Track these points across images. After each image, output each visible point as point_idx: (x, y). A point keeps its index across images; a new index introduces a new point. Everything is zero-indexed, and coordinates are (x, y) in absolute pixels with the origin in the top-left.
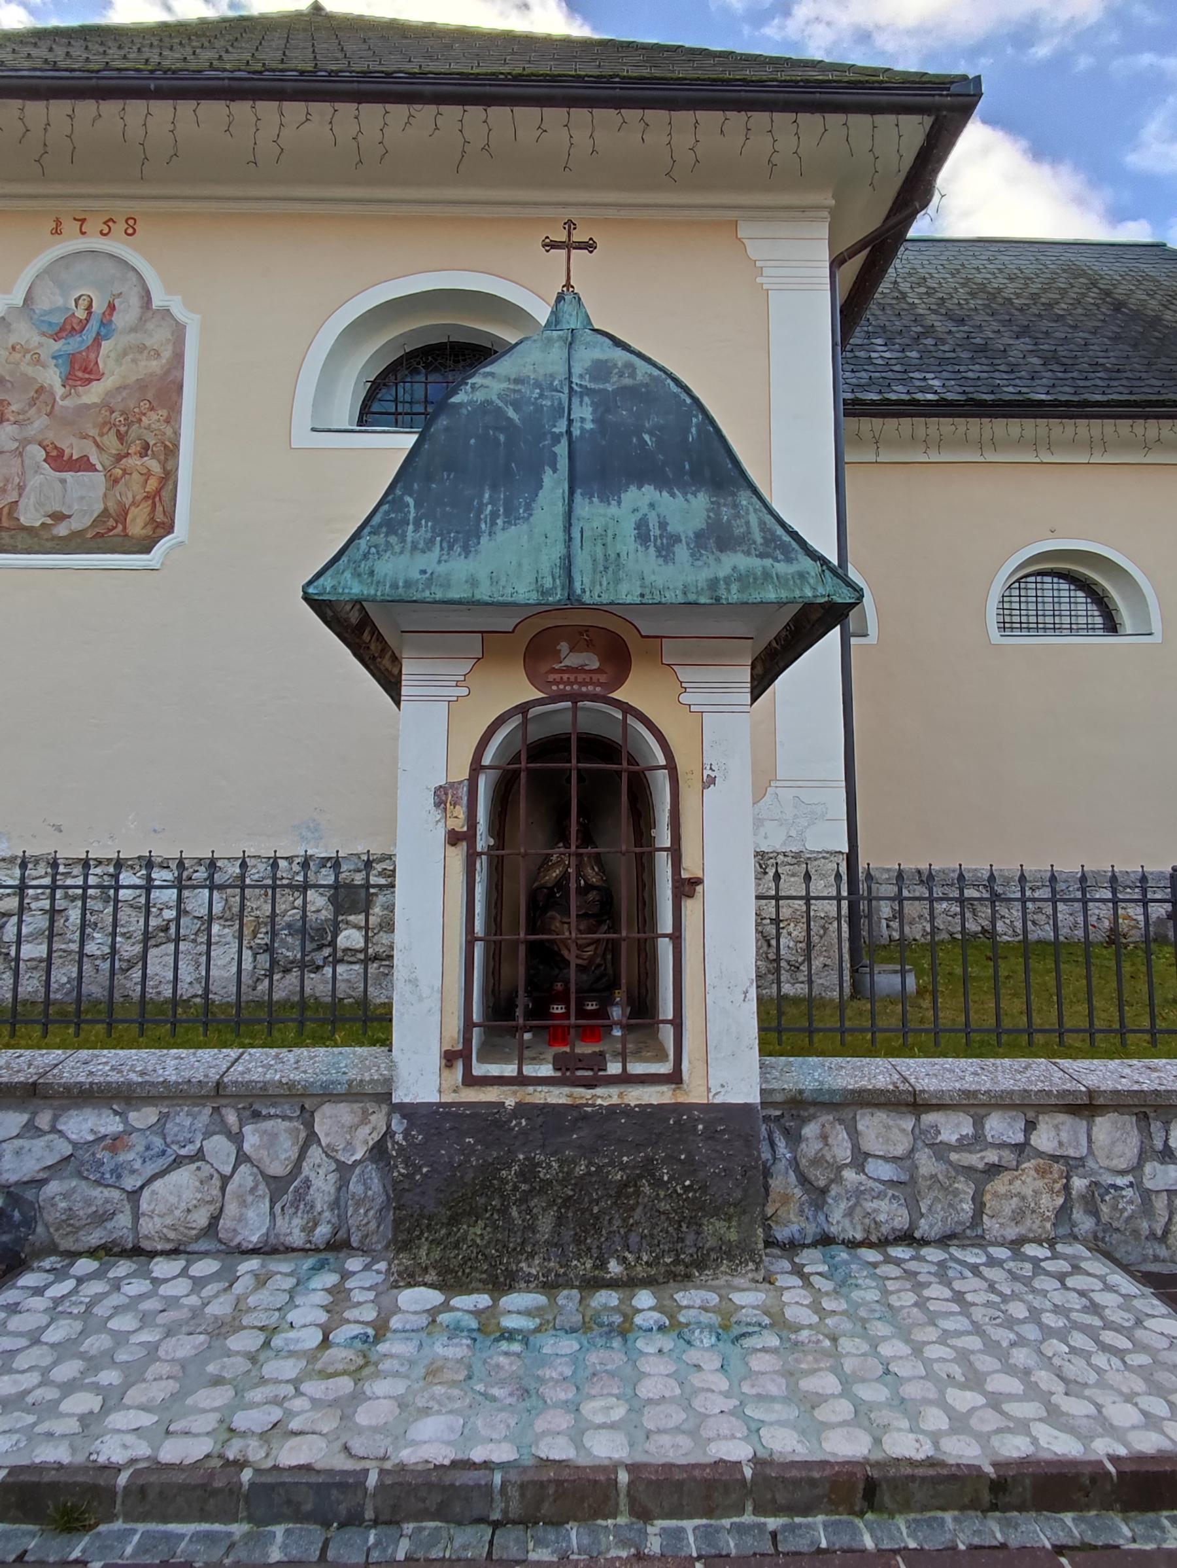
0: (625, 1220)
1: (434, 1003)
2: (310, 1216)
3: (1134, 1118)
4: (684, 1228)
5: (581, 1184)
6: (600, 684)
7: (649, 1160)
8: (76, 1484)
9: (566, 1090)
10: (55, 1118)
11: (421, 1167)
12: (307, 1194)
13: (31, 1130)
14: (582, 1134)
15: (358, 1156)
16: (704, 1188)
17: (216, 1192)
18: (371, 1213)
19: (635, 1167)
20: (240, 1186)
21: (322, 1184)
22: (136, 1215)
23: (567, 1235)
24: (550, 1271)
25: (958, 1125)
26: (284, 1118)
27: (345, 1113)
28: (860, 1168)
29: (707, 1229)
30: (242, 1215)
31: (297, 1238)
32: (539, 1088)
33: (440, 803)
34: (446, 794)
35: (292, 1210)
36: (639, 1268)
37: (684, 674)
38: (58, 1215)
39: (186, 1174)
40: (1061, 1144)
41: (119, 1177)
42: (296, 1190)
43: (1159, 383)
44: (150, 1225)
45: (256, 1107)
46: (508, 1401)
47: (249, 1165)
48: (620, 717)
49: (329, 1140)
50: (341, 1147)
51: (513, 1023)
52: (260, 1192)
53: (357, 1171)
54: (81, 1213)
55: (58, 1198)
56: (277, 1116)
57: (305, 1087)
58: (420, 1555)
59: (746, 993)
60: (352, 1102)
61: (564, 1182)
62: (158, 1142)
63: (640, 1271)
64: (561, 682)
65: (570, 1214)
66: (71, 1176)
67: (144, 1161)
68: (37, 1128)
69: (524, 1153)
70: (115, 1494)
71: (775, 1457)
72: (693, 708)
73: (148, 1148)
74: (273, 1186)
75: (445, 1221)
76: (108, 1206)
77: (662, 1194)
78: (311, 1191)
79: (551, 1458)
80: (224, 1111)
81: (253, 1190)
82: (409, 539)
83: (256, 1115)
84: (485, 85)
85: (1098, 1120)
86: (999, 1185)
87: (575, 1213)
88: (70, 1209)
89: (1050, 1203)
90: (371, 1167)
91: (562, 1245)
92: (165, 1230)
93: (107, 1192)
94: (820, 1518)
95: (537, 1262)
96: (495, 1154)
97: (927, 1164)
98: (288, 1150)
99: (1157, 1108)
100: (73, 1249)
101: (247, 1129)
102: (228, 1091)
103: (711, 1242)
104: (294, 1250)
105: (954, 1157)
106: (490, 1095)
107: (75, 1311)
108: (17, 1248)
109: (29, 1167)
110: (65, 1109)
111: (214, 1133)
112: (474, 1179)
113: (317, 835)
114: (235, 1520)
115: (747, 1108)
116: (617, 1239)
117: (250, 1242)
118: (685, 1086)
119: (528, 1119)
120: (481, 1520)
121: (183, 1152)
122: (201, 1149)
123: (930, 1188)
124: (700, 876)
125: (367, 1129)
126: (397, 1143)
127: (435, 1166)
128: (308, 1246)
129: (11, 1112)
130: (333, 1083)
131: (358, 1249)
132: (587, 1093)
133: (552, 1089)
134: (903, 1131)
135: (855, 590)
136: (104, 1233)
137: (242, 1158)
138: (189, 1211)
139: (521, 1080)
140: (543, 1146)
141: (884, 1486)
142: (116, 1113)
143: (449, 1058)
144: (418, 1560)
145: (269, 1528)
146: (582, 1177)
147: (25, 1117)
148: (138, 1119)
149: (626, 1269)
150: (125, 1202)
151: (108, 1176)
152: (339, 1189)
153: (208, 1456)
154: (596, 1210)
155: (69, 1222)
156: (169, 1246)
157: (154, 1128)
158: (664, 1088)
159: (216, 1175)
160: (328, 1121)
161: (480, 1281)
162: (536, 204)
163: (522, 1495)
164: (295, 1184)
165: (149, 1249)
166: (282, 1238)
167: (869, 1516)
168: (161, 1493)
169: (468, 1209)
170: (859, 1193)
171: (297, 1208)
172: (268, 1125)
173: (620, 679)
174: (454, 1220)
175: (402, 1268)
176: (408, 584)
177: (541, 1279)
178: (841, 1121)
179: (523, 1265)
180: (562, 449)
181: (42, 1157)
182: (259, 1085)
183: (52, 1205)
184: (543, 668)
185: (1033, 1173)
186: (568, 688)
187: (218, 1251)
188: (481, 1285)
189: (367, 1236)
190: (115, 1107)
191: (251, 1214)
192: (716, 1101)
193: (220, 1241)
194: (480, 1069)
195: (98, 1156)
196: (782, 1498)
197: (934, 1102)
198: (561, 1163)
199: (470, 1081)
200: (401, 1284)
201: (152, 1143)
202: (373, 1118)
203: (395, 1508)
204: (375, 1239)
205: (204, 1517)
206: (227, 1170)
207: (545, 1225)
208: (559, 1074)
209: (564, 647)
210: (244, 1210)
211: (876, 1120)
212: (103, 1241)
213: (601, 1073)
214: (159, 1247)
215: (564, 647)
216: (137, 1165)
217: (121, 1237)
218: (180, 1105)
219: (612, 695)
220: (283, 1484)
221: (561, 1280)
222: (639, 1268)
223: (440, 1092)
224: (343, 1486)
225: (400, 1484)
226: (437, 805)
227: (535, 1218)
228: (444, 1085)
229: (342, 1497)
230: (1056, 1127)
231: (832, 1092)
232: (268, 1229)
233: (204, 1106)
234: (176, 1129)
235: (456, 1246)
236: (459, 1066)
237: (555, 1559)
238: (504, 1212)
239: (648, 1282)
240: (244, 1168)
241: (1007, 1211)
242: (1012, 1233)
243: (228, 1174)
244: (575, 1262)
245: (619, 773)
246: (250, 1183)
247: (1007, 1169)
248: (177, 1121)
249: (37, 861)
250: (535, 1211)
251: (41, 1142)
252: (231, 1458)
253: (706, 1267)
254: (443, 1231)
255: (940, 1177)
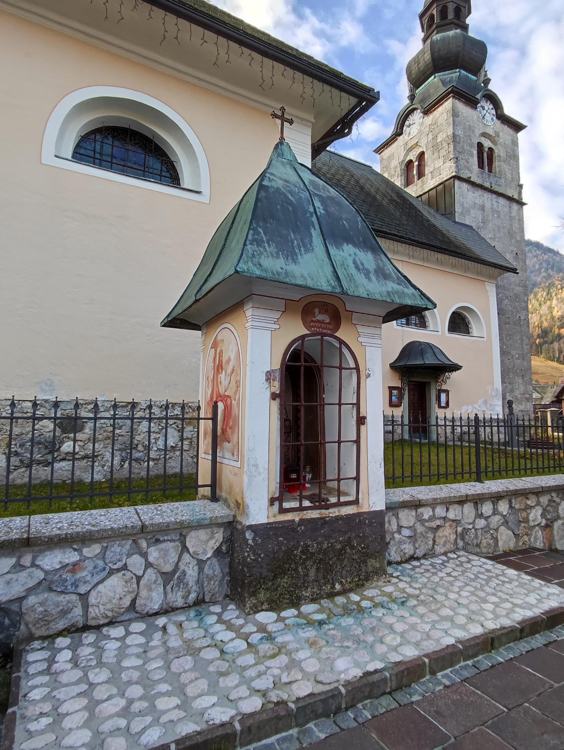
0: (341, 565)
1: (265, 475)
2: (187, 589)
3: (473, 504)
4: (362, 565)
5: (325, 552)
6: (330, 329)
7: (349, 538)
8: (217, 737)
9: (318, 511)
10: (34, 559)
11: (260, 555)
12: (184, 578)
13: (18, 567)
14: (325, 530)
15: (209, 555)
16: (368, 546)
17: (135, 586)
18: (217, 583)
19: (344, 542)
20: (148, 580)
21: (192, 572)
22: (86, 607)
23: (320, 575)
24: (314, 593)
25: (428, 512)
26: (171, 541)
27: (202, 534)
28: (399, 532)
29: (369, 564)
30: (149, 595)
31: (180, 602)
32: (309, 511)
33: (268, 379)
34: (270, 375)
35: (177, 589)
36: (347, 585)
37: (361, 329)
38: (37, 616)
39: (116, 579)
40: (456, 515)
41: (77, 587)
42: (179, 578)
43: (381, 224)
44: (97, 611)
45: (158, 537)
46: (354, 646)
47: (152, 569)
48: (338, 346)
49: (194, 549)
50: (201, 552)
51: (299, 483)
52: (159, 582)
53: (208, 563)
54: (54, 612)
55: (37, 605)
56: (168, 540)
57: (189, 523)
58: (376, 714)
59: (381, 464)
60: (206, 528)
61: (319, 553)
62: (101, 563)
63: (347, 586)
64: (315, 327)
65: (321, 566)
66: (43, 591)
67: (93, 575)
68: (21, 565)
69: (303, 542)
70: (236, 734)
71: (461, 639)
72: (363, 344)
73: (95, 567)
74: (164, 578)
75: (272, 578)
76: (70, 605)
77: (354, 552)
78: (187, 577)
79: (397, 661)
80: (140, 541)
81: (155, 582)
82: (268, 251)
83: (158, 541)
84: (181, 7)
85: (465, 505)
86: (440, 533)
87: (323, 565)
88: (46, 611)
89: (453, 537)
90: (214, 560)
91: (318, 581)
92: (106, 612)
93: (67, 597)
94: (481, 657)
95: (309, 590)
96: (292, 544)
97: (420, 529)
98: (173, 556)
99: (480, 499)
100: (44, 635)
101: (152, 549)
102: (148, 530)
103: (370, 569)
104: (177, 609)
105: (427, 524)
106: (289, 517)
107: (93, 664)
108: (8, 642)
109: (17, 590)
110: (41, 552)
111: (133, 554)
112: (283, 556)
113: (51, 388)
114: (290, 728)
115: (381, 511)
116: (339, 574)
117: (154, 609)
118: (360, 505)
119: (304, 526)
120: (384, 694)
121: (115, 567)
122: (125, 565)
123: (420, 537)
124: (365, 415)
125: (213, 541)
126: (249, 545)
127: (267, 553)
128: (185, 605)
129: (4, 558)
130: (202, 519)
131: (209, 602)
132: (326, 512)
133: (313, 511)
134: (412, 516)
135: (433, 304)
136: (66, 621)
137: (148, 565)
138: (121, 598)
139: (301, 509)
140: (310, 538)
141: (496, 639)
142: (75, 550)
143: (272, 501)
144: (377, 716)
145: (306, 726)
146: (325, 549)
147: (13, 561)
148: (89, 552)
149: (342, 586)
150: (78, 601)
151: (69, 587)
152: (199, 574)
153: (263, 705)
154: (331, 563)
155: (45, 619)
156: (106, 621)
157: (98, 556)
158: (353, 507)
159: (134, 577)
160: (194, 540)
161: (287, 603)
162: (185, 73)
163: (397, 678)
164: (177, 574)
165: (94, 624)
166: (171, 604)
167: (493, 651)
168: (258, 726)
169: (281, 571)
170: (400, 542)
171: (179, 587)
172: (163, 545)
173: (337, 328)
174: (275, 577)
175: (252, 605)
176: (279, 274)
177: (311, 597)
178: (393, 515)
179: (304, 592)
180: (314, 219)
181: (26, 583)
182: (165, 525)
183: (32, 611)
184: (309, 319)
185: (448, 527)
186: (318, 330)
187: (136, 618)
188: (287, 605)
189: (213, 595)
190: (75, 546)
191: (154, 594)
192: (372, 510)
193: (137, 612)
194: (286, 505)
195: (64, 577)
196: (470, 653)
197: (425, 503)
198: (318, 544)
199: (282, 511)
200: (251, 612)
201: (97, 564)
202: (216, 535)
203: (353, 700)
204: (217, 596)
205: (277, 732)
206: (140, 573)
207: (312, 573)
208: (313, 505)
209: (317, 311)
210: (150, 593)
211: (404, 513)
212: (66, 626)
213: (328, 503)
214: (101, 622)
215: (317, 311)
216: (88, 578)
217: (77, 621)
218: (113, 541)
219: (335, 334)
220: (310, 704)
221: (318, 596)
222: (347, 585)
223: (268, 518)
224: (333, 697)
225: (355, 688)
226: (267, 380)
227: (308, 570)
228: (270, 514)
229: (333, 702)
230: (454, 509)
231: (395, 503)
232: (162, 601)
233: (128, 539)
234: (112, 554)
235: (277, 590)
236: (277, 504)
237: (421, 698)
238: (296, 570)
239: (351, 590)
240: (150, 571)
241: (442, 542)
242: (442, 551)
243: (141, 575)
244: (324, 587)
245: (299, 367)
246: (154, 578)
247: (441, 527)
248: (112, 550)
249: (174, 405)
250: (308, 567)
251: (24, 574)
252: (276, 701)
253: (369, 580)
254: (270, 584)
255: (423, 533)
